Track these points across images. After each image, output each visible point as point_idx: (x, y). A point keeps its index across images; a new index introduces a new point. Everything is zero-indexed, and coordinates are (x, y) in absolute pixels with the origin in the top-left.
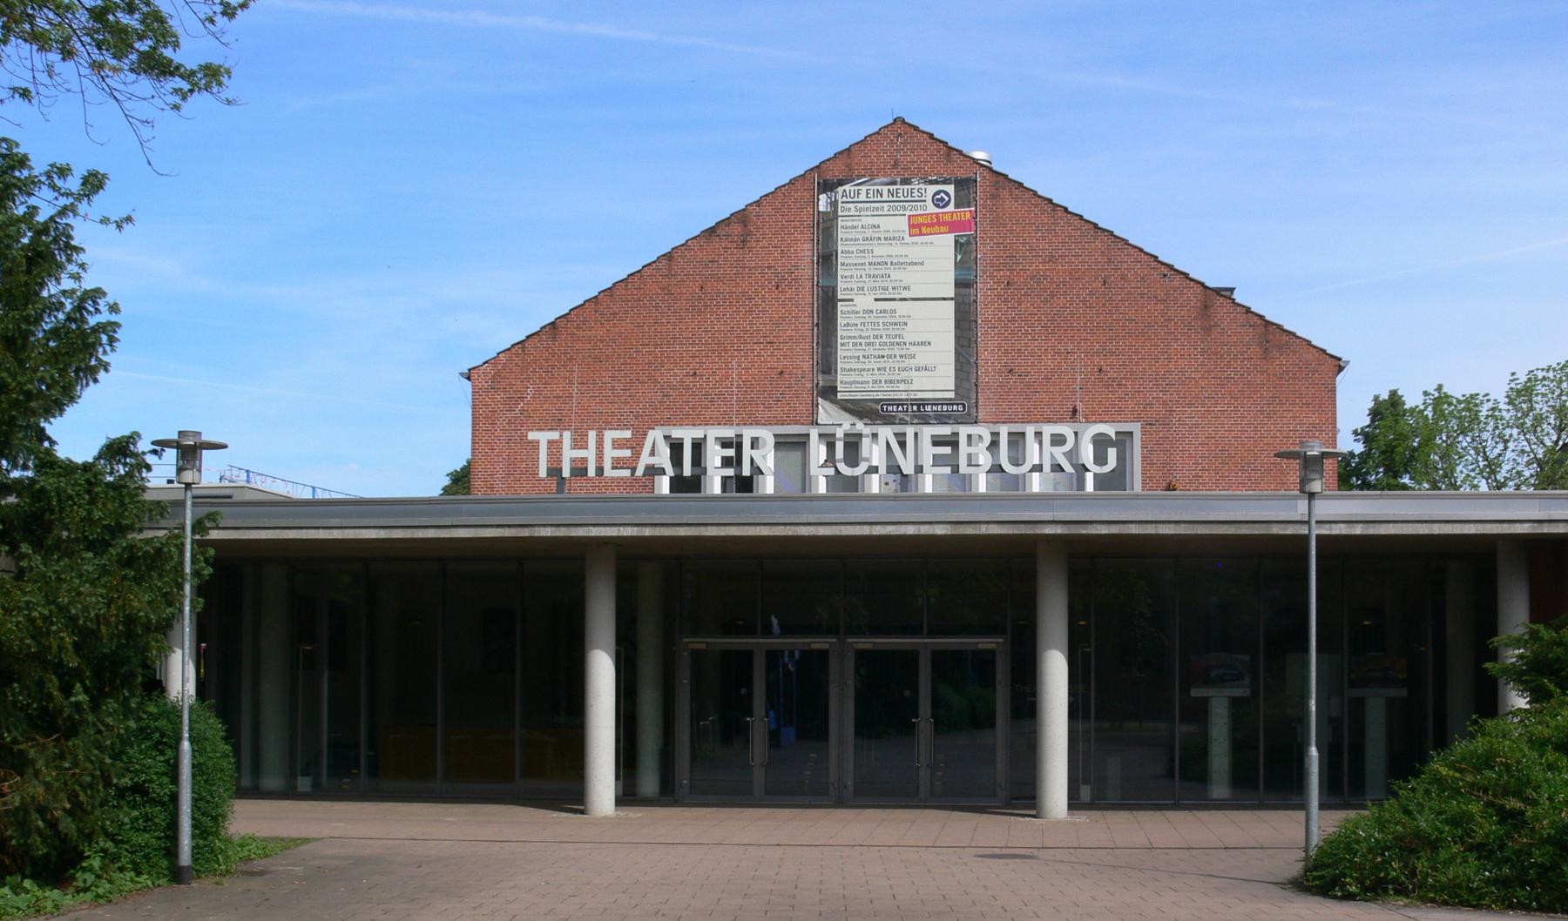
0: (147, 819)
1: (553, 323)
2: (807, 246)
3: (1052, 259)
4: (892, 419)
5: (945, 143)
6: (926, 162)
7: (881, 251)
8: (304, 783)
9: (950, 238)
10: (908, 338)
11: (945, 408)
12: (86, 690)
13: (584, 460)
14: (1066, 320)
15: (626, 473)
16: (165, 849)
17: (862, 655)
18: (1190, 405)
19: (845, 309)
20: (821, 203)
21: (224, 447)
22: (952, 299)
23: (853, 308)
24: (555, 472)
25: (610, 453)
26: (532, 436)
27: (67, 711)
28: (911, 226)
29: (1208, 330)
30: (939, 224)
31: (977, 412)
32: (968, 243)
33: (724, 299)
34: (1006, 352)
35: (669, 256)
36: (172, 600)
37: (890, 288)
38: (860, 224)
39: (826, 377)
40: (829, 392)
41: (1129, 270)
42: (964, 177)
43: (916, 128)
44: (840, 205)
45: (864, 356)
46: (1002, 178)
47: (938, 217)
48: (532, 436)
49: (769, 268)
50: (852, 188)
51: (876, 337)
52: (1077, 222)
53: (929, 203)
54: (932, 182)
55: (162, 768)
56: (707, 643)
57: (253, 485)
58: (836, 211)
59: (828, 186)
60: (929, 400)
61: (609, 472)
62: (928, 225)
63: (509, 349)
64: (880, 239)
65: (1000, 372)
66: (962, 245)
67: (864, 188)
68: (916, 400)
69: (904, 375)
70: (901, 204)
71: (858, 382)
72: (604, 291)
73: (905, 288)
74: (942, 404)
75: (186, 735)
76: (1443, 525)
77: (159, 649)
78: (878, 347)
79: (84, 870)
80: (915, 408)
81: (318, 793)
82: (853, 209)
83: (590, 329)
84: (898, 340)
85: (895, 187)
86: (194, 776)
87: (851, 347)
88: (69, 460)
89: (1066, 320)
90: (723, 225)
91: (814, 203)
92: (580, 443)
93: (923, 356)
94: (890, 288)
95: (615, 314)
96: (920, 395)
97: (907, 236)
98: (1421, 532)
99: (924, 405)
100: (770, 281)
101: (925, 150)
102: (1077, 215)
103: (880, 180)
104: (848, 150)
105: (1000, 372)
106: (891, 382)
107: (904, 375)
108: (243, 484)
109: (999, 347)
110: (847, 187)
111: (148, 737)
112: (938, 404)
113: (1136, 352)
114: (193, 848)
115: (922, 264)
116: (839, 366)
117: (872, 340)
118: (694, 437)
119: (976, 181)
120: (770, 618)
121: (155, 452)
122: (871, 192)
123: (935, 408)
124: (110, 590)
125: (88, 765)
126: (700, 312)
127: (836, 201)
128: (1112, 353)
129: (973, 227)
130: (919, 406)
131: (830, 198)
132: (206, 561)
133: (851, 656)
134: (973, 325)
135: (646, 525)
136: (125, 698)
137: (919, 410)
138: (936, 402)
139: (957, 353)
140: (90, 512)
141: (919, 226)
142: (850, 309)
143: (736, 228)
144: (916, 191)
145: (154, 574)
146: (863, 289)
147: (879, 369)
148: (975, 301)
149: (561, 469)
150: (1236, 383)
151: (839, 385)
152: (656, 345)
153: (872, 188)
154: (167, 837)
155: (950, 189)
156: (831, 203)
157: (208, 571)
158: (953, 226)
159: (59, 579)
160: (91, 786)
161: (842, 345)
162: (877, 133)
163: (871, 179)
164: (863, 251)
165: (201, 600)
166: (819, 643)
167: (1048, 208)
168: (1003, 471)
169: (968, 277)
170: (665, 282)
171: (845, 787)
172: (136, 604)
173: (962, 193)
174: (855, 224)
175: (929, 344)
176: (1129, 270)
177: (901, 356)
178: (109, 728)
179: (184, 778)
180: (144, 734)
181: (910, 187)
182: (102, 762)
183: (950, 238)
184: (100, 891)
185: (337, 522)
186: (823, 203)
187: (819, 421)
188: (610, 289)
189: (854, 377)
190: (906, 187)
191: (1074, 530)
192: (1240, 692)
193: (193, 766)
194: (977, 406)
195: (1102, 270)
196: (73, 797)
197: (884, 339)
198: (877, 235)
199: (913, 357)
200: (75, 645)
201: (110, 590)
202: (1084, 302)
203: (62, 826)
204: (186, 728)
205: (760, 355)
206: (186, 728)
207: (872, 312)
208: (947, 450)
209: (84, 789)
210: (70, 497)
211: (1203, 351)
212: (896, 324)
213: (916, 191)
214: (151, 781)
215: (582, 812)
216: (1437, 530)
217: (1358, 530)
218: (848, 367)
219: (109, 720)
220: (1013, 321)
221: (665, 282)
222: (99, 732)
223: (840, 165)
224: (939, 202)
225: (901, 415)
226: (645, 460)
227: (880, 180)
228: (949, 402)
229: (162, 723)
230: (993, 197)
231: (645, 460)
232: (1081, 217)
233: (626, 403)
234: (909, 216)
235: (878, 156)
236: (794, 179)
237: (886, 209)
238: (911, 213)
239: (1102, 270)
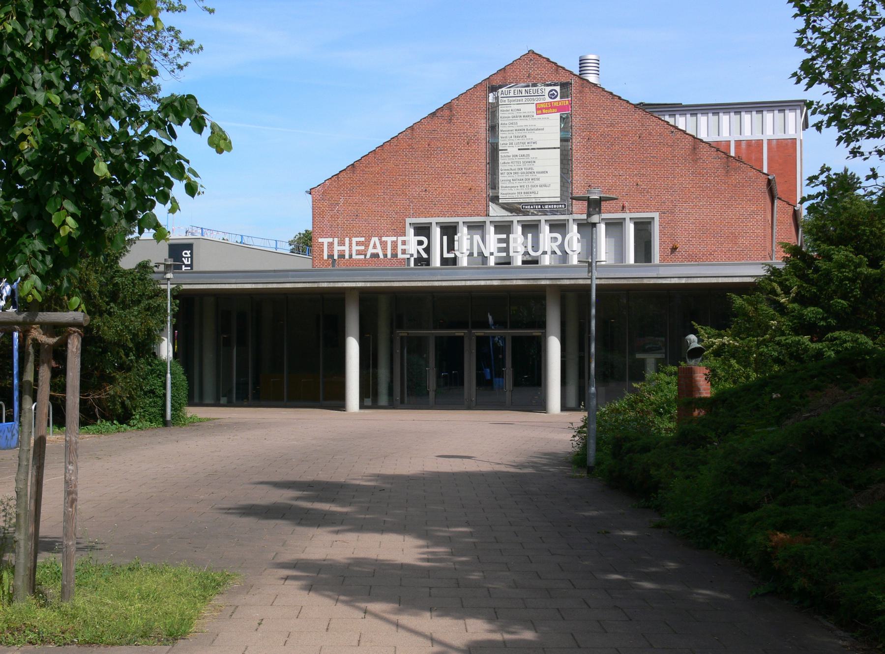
0: (155, 403)
1: (353, 165)
2: (484, 121)
3: (612, 125)
4: (528, 213)
5: (555, 64)
6: (545, 74)
7: (521, 123)
8: (223, 400)
9: (558, 115)
10: (535, 170)
11: (555, 206)
12: (134, 355)
13: (344, 251)
14: (619, 158)
15: (362, 257)
16: (162, 414)
17: (478, 338)
18: (685, 202)
19: (503, 155)
20: (490, 98)
22: (559, 148)
23: (507, 154)
24: (331, 256)
25: (355, 248)
26: (320, 240)
27: (128, 363)
28: (537, 109)
29: (695, 161)
30: (552, 108)
31: (572, 208)
32: (567, 118)
33: (441, 151)
34: (587, 176)
35: (412, 128)
36: (164, 322)
37: (526, 143)
38: (510, 109)
39: (494, 191)
40: (495, 199)
41: (653, 130)
42: (565, 81)
43: (540, 56)
44: (500, 99)
45: (513, 180)
46: (585, 81)
47: (551, 104)
48: (320, 240)
49: (464, 133)
50: (506, 90)
51: (519, 169)
52: (625, 104)
53: (547, 96)
54: (548, 85)
55: (160, 384)
56: (408, 333)
57: (205, 237)
58: (498, 102)
59: (494, 89)
60: (547, 202)
61: (354, 256)
62: (546, 108)
63: (330, 178)
64: (521, 116)
65: (584, 187)
66: (564, 119)
67: (512, 89)
68: (540, 202)
69: (534, 189)
70: (532, 97)
71: (510, 194)
72: (379, 147)
73: (534, 143)
74: (554, 205)
75: (169, 372)
76: (723, 278)
77: (159, 340)
78: (520, 175)
79: (133, 419)
80: (539, 207)
81: (230, 404)
82: (507, 101)
83: (372, 167)
84: (530, 171)
85: (529, 88)
86: (172, 387)
87: (506, 175)
89: (619, 158)
90: (440, 111)
91: (487, 98)
92: (342, 243)
93: (543, 179)
94: (526, 143)
95: (384, 159)
96: (542, 200)
97: (535, 114)
98: (713, 282)
99: (544, 205)
100: (464, 140)
101: (545, 67)
102: (625, 100)
103: (521, 85)
104: (504, 69)
105: (584, 187)
106: (527, 193)
107: (534, 189)
108: (199, 236)
109: (584, 173)
110: (503, 89)
111: (155, 373)
112: (551, 205)
113: (657, 174)
114: (172, 415)
115: (543, 129)
116: (500, 185)
117: (517, 171)
119: (571, 84)
121: (156, 266)
122: (516, 91)
123: (550, 207)
124: (142, 319)
125: (135, 381)
126: (428, 157)
127: (498, 97)
128: (644, 175)
129: (570, 109)
130: (541, 205)
131: (495, 95)
132: (176, 305)
133: (474, 338)
134: (570, 162)
135: (368, 282)
136: (147, 358)
137: (541, 208)
138: (550, 203)
139: (561, 177)
140: (133, 290)
141: (541, 109)
142: (505, 154)
143: (446, 112)
144: (539, 90)
145: (157, 313)
146: (512, 144)
147: (521, 186)
148: (571, 149)
149: (333, 255)
150: (711, 190)
151: (500, 195)
152: (406, 175)
153: (517, 89)
154: (162, 410)
155: (558, 88)
156: (495, 98)
157: (177, 309)
158: (559, 109)
159: (126, 317)
160: (136, 389)
161: (501, 174)
162: (519, 59)
163: (516, 85)
164: (512, 124)
165: (175, 319)
166: (459, 333)
167: (610, 97)
168: (529, 254)
169: (567, 136)
170: (410, 142)
171: (471, 400)
172: (151, 324)
173: (564, 90)
174: (508, 109)
175: (547, 172)
176: (653, 130)
177: (532, 179)
178: (142, 369)
180: (152, 372)
181: (536, 88)
182: (139, 381)
183: (558, 115)
184: (139, 426)
185: (234, 281)
186: (491, 98)
187: (490, 215)
188: (382, 146)
189: (508, 191)
190: (534, 88)
191: (555, 282)
192: (659, 356)
193: (172, 383)
194: (572, 205)
195: (639, 130)
196: (130, 393)
197: (523, 171)
198: (519, 115)
199: (538, 179)
200: (131, 339)
201: (142, 319)
202: (629, 148)
203: (126, 403)
204: (169, 369)
205: (459, 180)
206: (169, 369)
207: (517, 156)
208: (504, 245)
209: (133, 390)
210: (126, 285)
211: (693, 173)
212: (529, 162)
213: (539, 90)
214: (156, 389)
215: (344, 411)
216: (720, 280)
217: (683, 281)
218: (504, 186)
219: (142, 366)
220: (591, 159)
221: (410, 142)
222: (138, 370)
223: (500, 77)
224: (552, 96)
225: (532, 211)
226: (371, 250)
227: (521, 85)
228: (557, 203)
229: (160, 367)
230: (580, 92)
231: (371, 250)
232: (628, 102)
233: (390, 206)
234: (536, 104)
235: (520, 72)
236: (476, 85)
237: (524, 100)
238: (539, 102)
239: (639, 130)
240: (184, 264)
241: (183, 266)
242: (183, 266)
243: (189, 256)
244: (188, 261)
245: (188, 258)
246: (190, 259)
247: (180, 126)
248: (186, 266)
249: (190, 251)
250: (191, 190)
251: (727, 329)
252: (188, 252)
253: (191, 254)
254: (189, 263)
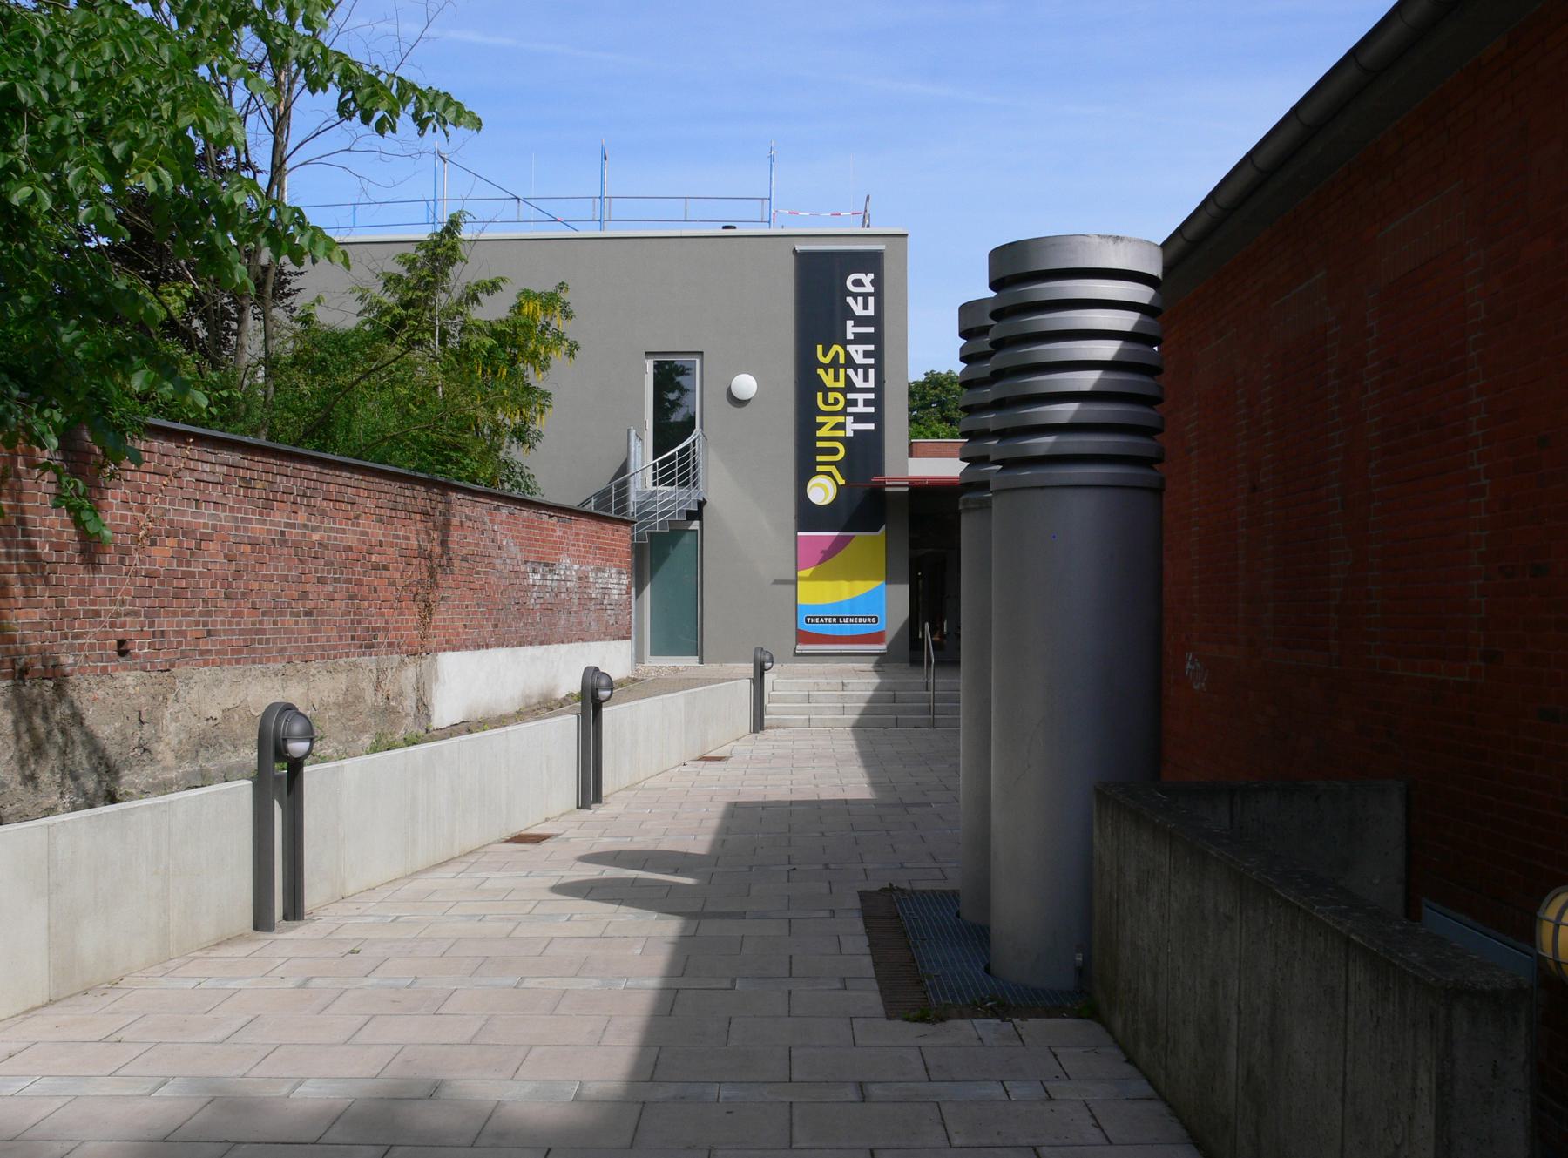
137: (838, 622)
240: (851, 315)
241: (850, 323)
242: (850, 323)
243: (871, 289)
244: (836, 379)
245: (866, 296)
246: (871, 300)
248: (860, 321)
249: (871, 276)
252: (867, 279)
254: (871, 312)
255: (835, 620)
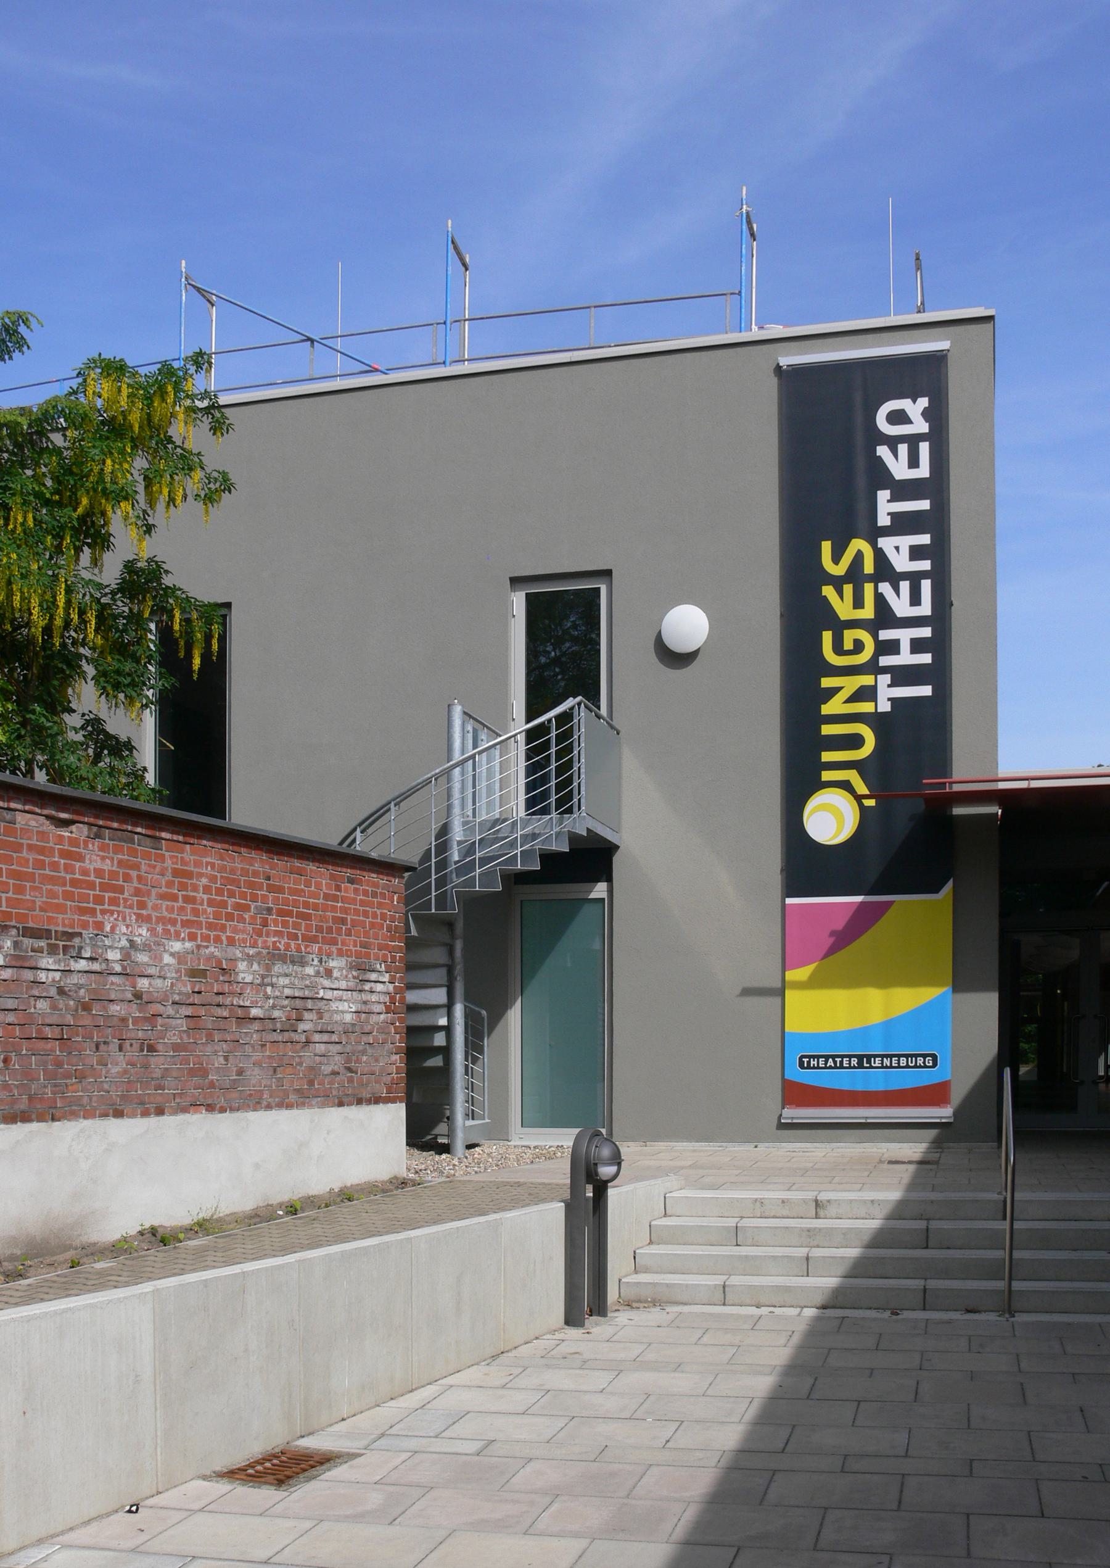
21: (917, 255)
88: (782, 870)
118: (237, 620)
120: (425, 1067)
179: (458, 1039)
241: (883, 495)
244: (914, 463)
245: (913, 441)
246: (924, 448)
247: (617, 860)
248: (904, 490)
249: (923, 402)
250: (29, 347)
251: (138, 655)
252: (915, 408)
253: (936, 415)
254: (923, 471)
255: (854, 1061)
